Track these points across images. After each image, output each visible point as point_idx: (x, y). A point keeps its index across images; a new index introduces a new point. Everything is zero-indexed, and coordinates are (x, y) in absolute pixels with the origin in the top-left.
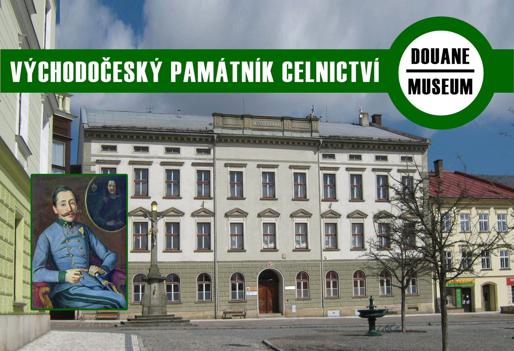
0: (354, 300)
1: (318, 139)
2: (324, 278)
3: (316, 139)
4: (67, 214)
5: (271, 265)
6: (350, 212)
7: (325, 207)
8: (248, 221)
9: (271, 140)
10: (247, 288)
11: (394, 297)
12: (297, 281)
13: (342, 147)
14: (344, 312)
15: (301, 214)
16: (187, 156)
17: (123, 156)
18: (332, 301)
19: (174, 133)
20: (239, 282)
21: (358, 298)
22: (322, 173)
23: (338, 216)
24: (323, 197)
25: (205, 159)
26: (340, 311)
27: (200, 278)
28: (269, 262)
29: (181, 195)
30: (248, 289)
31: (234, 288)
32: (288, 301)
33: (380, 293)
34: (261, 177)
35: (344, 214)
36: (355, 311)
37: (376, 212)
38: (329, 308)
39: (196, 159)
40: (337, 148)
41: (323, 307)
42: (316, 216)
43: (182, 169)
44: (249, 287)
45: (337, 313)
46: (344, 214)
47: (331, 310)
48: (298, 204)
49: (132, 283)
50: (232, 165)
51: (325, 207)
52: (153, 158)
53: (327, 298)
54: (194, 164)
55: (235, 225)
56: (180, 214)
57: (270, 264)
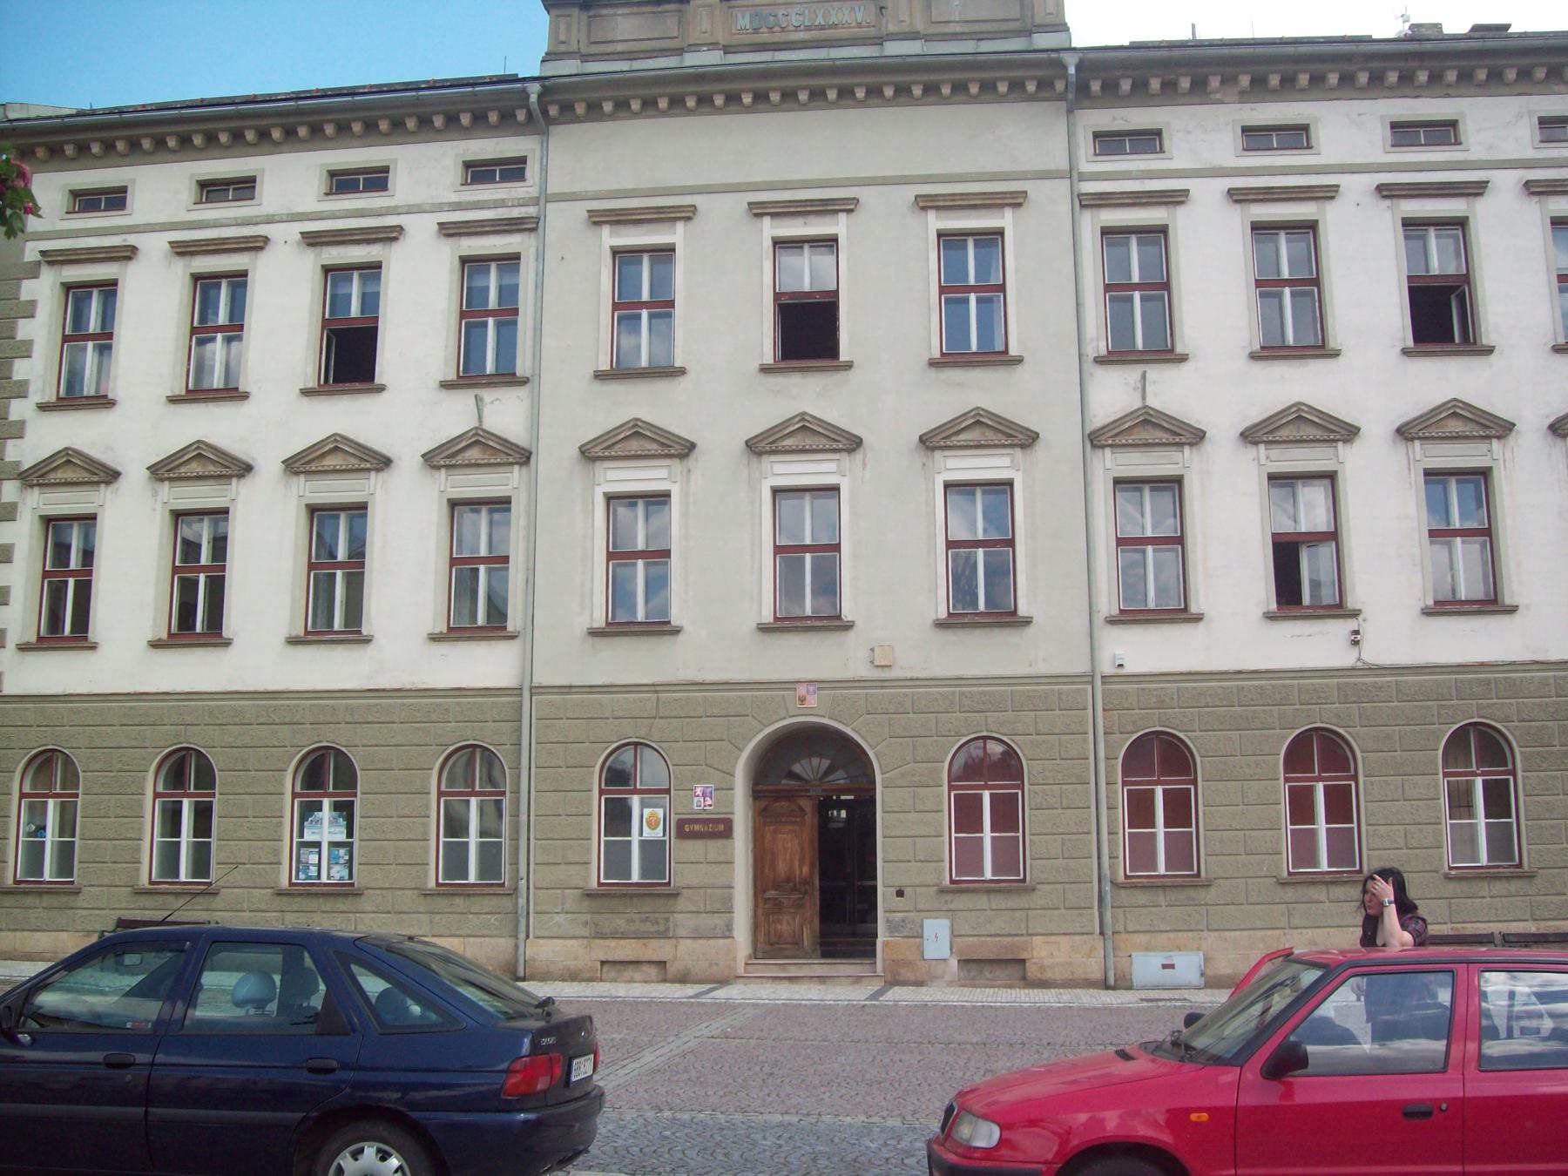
0: (1289, 893)
1: (1054, 55)
2: (150, 783)
3: (1044, 56)
5: (812, 701)
6: (1256, 415)
8: (692, 483)
11: (1530, 877)
12: (1445, 775)
13: (1199, 91)
15: (196, 468)
16: (420, 196)
17: (148, 228)
18: (1161, 898)
19: (349, 99)
21: (1313, 883)
22: (1091, 222)
23: (1189, 436)
24: (1098, 344)
25: (501, 204)
26: (1206, 960)
27: (1298, 756)
28: (802, 690)
32: (900, 894)
33: (1447, 858)
34: (933, 255)
35: (407, 456)
37: (1409, 410)
38: (1143, 938)
39: (458, 207)
40: (1169, 93)
41: (1102, 933)
43: (1332, 218)
46: (407, 456)
47: (1148, 948)
49: (1438, 770)
50: (619, 219)
52: (270, 220)
53: (1129, 885)
56: (1496, 428)
57: (802, 700)
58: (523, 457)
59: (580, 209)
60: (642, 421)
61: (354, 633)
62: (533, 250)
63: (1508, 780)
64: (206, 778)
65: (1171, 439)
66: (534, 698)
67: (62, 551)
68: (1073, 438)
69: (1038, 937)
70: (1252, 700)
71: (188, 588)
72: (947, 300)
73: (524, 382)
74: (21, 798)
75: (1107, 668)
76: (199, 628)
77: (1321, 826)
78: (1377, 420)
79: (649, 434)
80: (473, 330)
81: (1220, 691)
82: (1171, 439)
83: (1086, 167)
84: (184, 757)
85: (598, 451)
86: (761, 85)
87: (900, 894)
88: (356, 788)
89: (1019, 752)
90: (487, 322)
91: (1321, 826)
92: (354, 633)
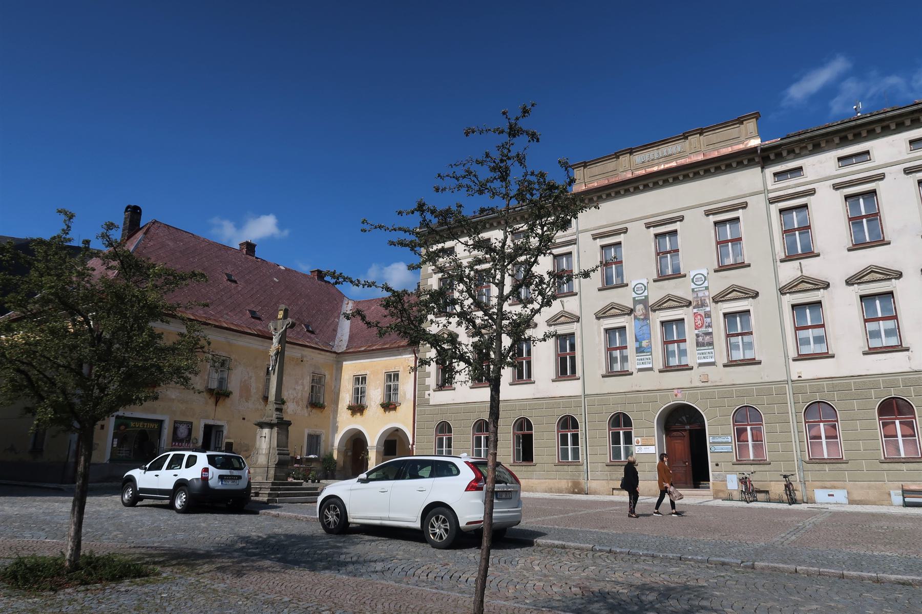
0: (885, 466)
4: (641, 315)
5: (679, 396)
6: (852, 272)
7: (789, 272)
9: (739, 159)
10: (636, 439)
14: (856, 496)
15: (563, 319)
20: (613, 430)
22: (774, 208)
26: (848, 493)
28: (676, 391)
29: (888, 235)
30: (638, 442)
31: (616, 440)
32: (717, 465)
36: (889, 494)
39: (910, 160)
42: (768, 292)
44: (639, 439)
45: (840, 496)
48: (726, 277)
51: (789, 272)
54: (837, 187)
55: (673, 323)
57: (676, 395)
58: (578, 320)
59: (589, 234)
60: (614, 303)
61: (529, 380)
62: (576, 250)
63: (913, 421)
64: (575, 425)
65: (885, 277)
66: (586, 399)
67: (563, 348)
68: (774, 292)
69: (774, 482)
70: (860, 387)
71: (563, 361)
72: (852, 223)
73: (576, 294)
74: (879, 421)
75: (794, 377)
76: (568, 374)
77: (622, 445)
78: (837, 277)
79: (616, 307)
80: (662, 259)
81: (914, 379)
82: (885, 277)
83: (770, 187)
84: (619, 415)
85: (600, 315)
86: (645, 182)
87: (717, 465)
88: (632, 426)
89: (911, 403)
90: (667, 256)
91: (622, 445)
92: (529, 380)
